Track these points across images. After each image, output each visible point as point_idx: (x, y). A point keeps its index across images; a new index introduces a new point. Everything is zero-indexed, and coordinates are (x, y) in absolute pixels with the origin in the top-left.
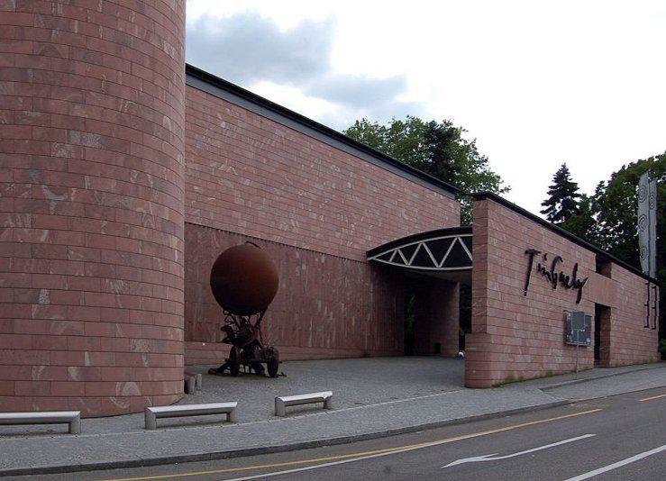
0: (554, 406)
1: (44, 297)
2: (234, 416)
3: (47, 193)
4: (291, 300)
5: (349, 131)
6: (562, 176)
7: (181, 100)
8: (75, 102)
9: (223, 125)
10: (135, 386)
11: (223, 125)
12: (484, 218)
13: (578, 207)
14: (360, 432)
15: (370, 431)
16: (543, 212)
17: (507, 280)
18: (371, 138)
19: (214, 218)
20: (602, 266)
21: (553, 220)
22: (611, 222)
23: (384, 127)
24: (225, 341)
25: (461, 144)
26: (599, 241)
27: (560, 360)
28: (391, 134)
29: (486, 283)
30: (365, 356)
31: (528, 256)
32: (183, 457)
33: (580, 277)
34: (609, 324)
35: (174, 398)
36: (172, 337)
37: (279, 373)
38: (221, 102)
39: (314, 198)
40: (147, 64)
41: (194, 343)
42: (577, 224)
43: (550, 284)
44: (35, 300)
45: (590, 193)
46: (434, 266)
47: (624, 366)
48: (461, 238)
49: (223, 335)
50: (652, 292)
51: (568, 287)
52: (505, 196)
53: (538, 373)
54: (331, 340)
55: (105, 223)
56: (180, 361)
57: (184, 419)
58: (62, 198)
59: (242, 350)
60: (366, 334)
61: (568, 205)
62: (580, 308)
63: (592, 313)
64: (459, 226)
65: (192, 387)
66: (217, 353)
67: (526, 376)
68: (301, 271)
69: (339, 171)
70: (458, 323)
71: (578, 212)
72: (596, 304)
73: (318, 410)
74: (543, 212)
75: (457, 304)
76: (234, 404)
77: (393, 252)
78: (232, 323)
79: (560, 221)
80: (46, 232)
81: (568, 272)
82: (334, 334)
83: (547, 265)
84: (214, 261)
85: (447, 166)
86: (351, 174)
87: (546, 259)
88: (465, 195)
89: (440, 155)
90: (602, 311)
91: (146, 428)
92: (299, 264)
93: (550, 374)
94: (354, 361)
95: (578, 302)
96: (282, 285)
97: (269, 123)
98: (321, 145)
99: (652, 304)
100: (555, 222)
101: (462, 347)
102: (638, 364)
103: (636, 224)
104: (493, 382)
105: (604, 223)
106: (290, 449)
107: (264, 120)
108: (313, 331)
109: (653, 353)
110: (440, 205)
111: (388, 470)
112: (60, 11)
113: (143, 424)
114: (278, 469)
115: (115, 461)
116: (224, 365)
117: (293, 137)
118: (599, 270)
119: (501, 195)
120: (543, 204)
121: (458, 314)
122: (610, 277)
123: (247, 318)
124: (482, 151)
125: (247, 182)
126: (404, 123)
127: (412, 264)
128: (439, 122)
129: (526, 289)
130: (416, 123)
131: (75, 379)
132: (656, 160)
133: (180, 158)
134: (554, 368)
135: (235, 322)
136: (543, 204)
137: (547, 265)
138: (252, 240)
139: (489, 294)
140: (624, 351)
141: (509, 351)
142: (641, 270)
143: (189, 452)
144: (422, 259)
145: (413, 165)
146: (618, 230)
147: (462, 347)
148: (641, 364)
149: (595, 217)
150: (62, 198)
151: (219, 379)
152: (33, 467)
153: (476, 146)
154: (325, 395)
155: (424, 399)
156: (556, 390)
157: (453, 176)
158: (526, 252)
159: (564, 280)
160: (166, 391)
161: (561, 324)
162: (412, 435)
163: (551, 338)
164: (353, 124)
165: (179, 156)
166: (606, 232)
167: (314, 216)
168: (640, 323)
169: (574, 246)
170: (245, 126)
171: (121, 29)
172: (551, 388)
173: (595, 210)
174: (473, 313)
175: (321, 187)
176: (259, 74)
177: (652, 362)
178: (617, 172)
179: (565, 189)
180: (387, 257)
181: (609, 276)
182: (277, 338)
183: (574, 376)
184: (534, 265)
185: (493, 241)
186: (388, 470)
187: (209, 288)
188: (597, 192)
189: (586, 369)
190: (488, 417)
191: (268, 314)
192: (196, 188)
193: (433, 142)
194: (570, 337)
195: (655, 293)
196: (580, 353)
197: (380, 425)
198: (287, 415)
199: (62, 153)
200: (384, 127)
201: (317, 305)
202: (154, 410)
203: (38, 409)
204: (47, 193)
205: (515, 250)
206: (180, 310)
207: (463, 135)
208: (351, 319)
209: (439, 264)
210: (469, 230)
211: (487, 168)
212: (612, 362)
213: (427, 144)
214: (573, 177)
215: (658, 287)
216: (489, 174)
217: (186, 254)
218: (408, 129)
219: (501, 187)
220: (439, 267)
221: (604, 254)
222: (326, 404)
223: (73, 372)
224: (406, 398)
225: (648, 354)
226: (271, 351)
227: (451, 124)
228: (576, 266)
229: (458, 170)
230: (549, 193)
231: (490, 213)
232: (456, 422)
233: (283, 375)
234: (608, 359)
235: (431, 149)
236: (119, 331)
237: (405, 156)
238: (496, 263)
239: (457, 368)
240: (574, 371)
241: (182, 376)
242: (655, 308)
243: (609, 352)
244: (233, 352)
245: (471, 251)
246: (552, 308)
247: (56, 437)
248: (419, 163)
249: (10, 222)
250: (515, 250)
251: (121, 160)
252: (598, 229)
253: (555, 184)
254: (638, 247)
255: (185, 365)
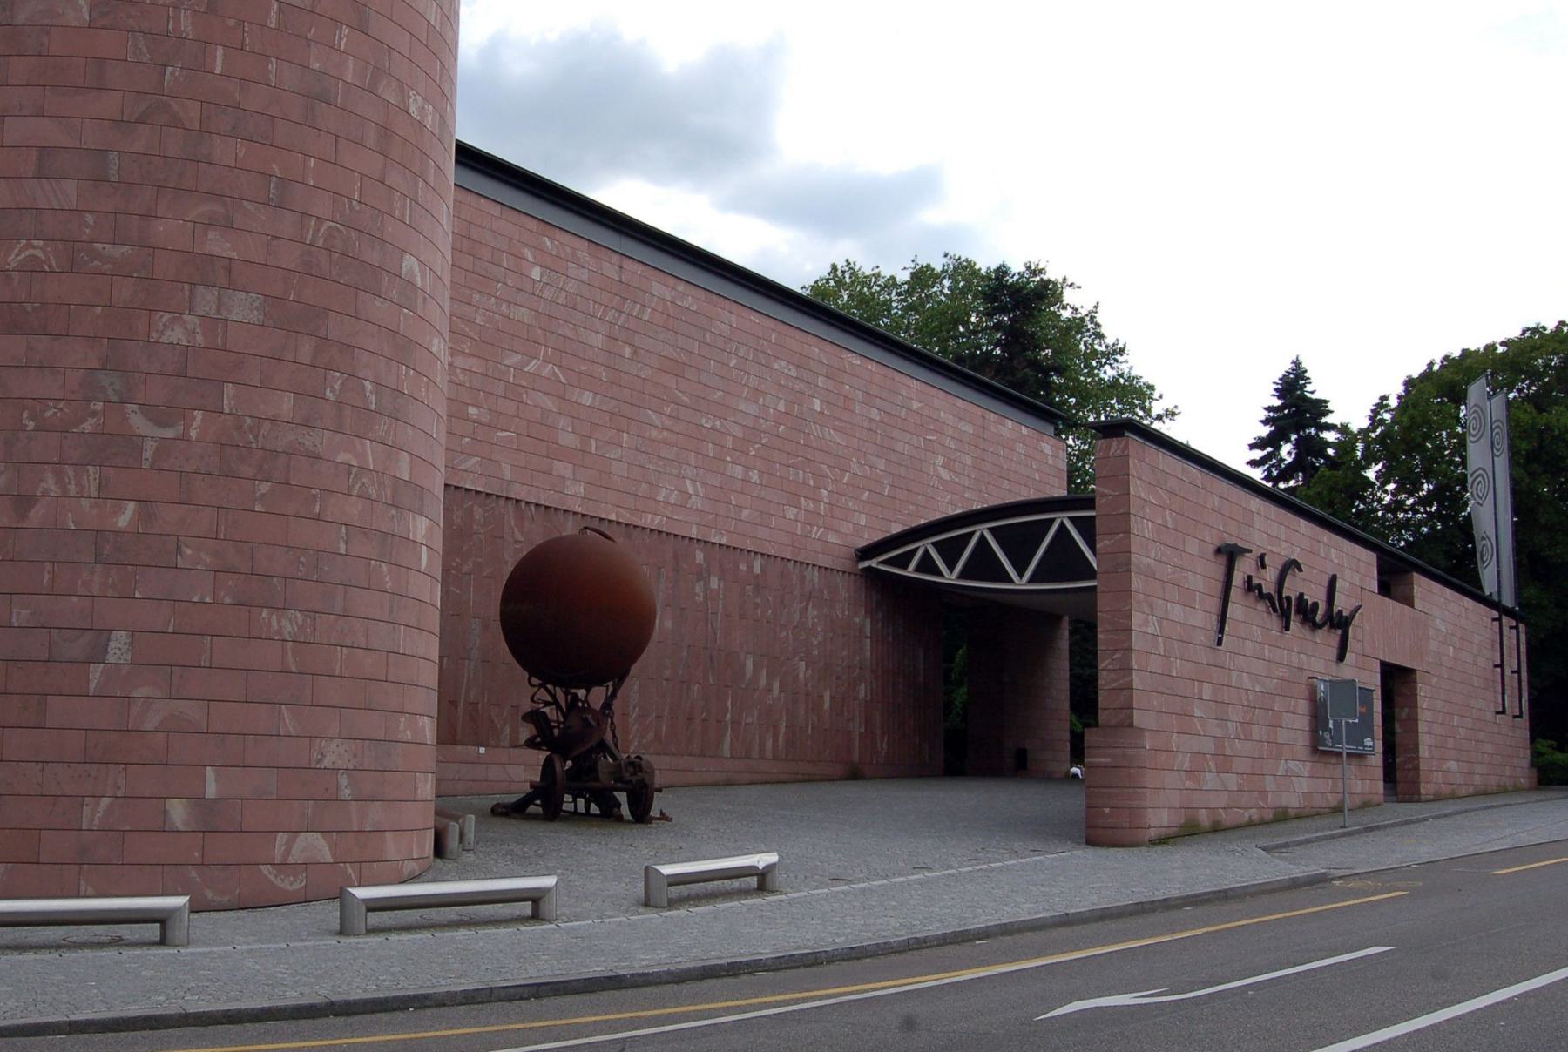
0: (1294, 884)
1: (118, 649)
2: (547, 907)
3: (138, 422)
4: (685, 654)
5: (815, 288)
6: (1292, 386)
7: (445, 221)
8: (211, 224)
9: (536, 273)
10: (319, 840)
11: (536, 273)
12: (1121, 479)
13: (1330, 451)
14: (842, 942)
15: (866, 939)
16: (1253, 463)
17: (1177, 612)
18: (864, 301)
19: (508, 475)
20: (1392, 580)
21: (1276, 481)
22: (1409, 484)
23: (893, 278)
24: (531, 744)
25: (1066, 314)
26: (1383, 525)
27: (1303, 785)
28: (909, 293)
29: (1130, 617)
30: (854, 774)
31: (1223, 560)
32: (427, 997)
33: (1342, 603)
34: (1414, 706)
35: (410, 867)
36: (409, 736)
37: (654, 812)
38: (532, 224)
39: (738, 431)
40: (371, 139)
41: (459, 748)
42: (1332, 489)
43: (1274, 622)
44: (97, 654)
45: (1359, 422)
46: (1011, 581)
47: (1453, 797)
48: (1071, 519)
49: (526, 731)
50: (1510, 637)
51: (1316, 626)
52: (1166, 428)
53: (1254, 814)
54: (775, 741)
55: (265, 487)
56: (426, 788)
57: (432, 914)
58: (169, 433)
59: (569, 763)
60: (857, 728)
61: (1310, 448)
62: (1347, 671)
63: (1373, 681)
64: (1065, 493)
65: (452, 842)
66: (511, 769)
67: (1227, 818)
68: (706, 588)
69: (793, 373)
70: (1067, 705)
71: (1332, 464)
72: (1383, 664)
73: (744, 893)
74: (1253, 463)
75: (1065, 664)
76: (549, 881)
77: (916, 550)
78: (547, 704)
79: (1292, 483)
80: (131, 506)
81: (1316, 595)
82: (783, 729)
83: (1268, 579)
84: (509, 569)
85: (1036, 364)
86: (821, 381)
87: (1263, 566)
88: (1076, 425)
89: (1018, 340)
90: (1396, 679)
91: (342, 932)
92: (702, 575)
93: (1282, 816)
94: (827, 787)
95: (1341, 657)
96: (664, 623)
97: (639, 269)
98: (755, 318)
99: (1511, 663)
100: (1282, 485)
101: (1077, 755)
102: (1486, 794)
103: (1464, 489)
104: (1153, 833)
105: (1391, 487)
106: (679, 977)
107: (627, 264)
108: (736, 723)
109: (1520, 764)
110: (1020, 448)
111: (909, 1024)
112: (186, 25)
113: (336, 925)
114: (649, 1022)
115: (266, 1004)
116: (528, 795)
117: (691, 299)
118: (1385, 589)
119: (1157, 425)
120: (1252, 447)
121: (1067, 685)
122: (1411, 605)
123: (581, 693)
124: (1113, 331)
125: (587, 398)
126: (938, 269)
127: (962, 576)
128: (1016, 267)
129: (1221, 630)
130: (964, 270)
131: (180, 826)
132: (1500, 349)
133: (438, 346)
134: (1293, 802)
135: (556, 702)
136: (1252, 447)
137: (1268, 579)
138: (595, 524)
139: (1136, 641)
140: (1453, 765)
141: (1187, 765)
142: (1481, 588)
143: (443, 986)
144: (983, 564)
145: (959, 359)
146: (1425, 501)
147: (1077, 755)
148: (1491, 794)
149: (1371, 474)
150: (169, 433)
151: (514, 827)
152: (73, 1017)
153: (1099, 319)
154: (762, 860)
155: (993, 870)
156: (1298, 851)
157: (1048, 386)
158: (1219, 551)
159: (1306, 612)
160: (391, 852)
161: (1303, 706)
162: (965, 949)
163: (1282, 736)
164: (824, 271)
165: (436, 341)
166: (1397, 506)
167: (738, 471)
168: (1486, 702)
169: (1327, 536)
170: (585, 275)
171: (317, 66)
172: (1286, 845)
173: (1370, 458)
174: (1101, 682)
175: (753, 409)
176: (616, 162)
177: (1517, 790)
178: (1415, 376)
179: (1299, 413)
180: (903, 561)
181: (1408, 601)
182: (651, 736)
183: (1339, 819)
184: (1238, 579)
185: (1142, 527)
186: (909, 1024)
187: (497, 628)
188: (1372, 419)
189: (1366, 805)
190: (1141, 909)
191: (632, 687)
192: (472, 410)
193: (1003, 310)
194: (1327, 736)
195: (1515, 638)
196: (1352, 769)
197: (888, 927)
198: (673, 904)
199: (176, 335)
200: (893, 278)
201: (743, 666)
202: (361, 893)
203: (90, 891)
204: (138, 422)
205: (1192, 547)
206: (429, 675)
207: (1069, 296)
208: (821, 697)
209: (1021, 575)
210: (1089, 503)
211: (1124, 368)
212: (1426, 789)
213: (989, 315)
214: (1317, 388)
215: (1522, 627)
216: (1130, 379)
217: (447, 554)
218: (947, 283)
219: (1157, 408)
220: (1020, 583)
221: (1393, 555)
222: (763, 881)
223: (178, 811)
224: (949, 867)
225: (1508, 771)
226: (636, 765)
227: (1041, 271)
228: (1333, 581)
229: (1060, 371)
230: (1265, 422)
231: (1133, 464)
232: (1066, 921)
233: (663, 817)
234: (1415, 783)
235: (999, 326)
236: (288, 721)
237: (943, 342)
238: (1149, 575)
239: (1070, 802)
240: (1338, 809)
241: (431, 821)
242: (1518, 672)
243: (1417, 768)
244: (548, 766)
245: (1093, 549)
246: (1282, 672)
247: (128, 953)
248: (973, 356)
249: (50, 484)
250: (1192, 547)
251: (305, 350)
252: (1380, 500)
253: (1277, 402)
254: (1471, 539)
255: (437, 796)
